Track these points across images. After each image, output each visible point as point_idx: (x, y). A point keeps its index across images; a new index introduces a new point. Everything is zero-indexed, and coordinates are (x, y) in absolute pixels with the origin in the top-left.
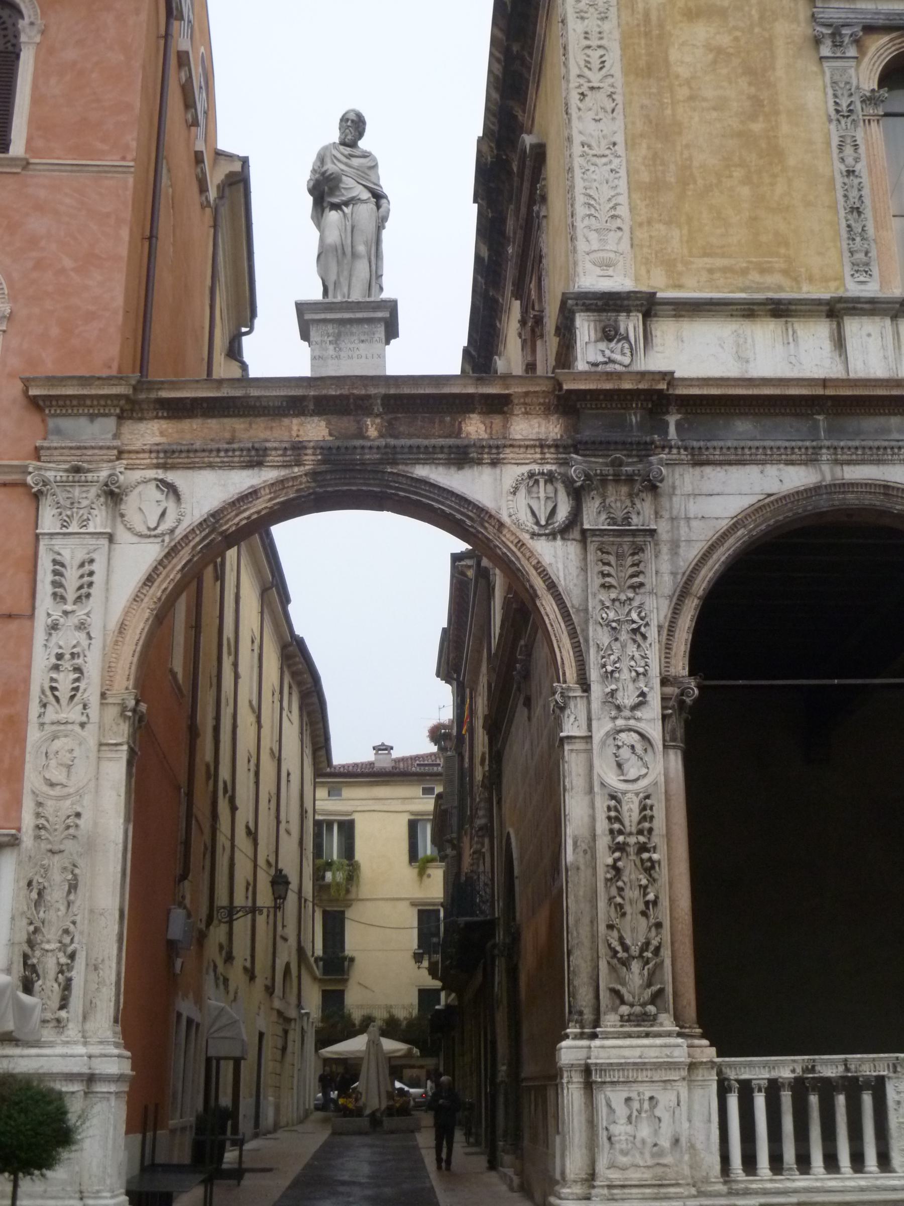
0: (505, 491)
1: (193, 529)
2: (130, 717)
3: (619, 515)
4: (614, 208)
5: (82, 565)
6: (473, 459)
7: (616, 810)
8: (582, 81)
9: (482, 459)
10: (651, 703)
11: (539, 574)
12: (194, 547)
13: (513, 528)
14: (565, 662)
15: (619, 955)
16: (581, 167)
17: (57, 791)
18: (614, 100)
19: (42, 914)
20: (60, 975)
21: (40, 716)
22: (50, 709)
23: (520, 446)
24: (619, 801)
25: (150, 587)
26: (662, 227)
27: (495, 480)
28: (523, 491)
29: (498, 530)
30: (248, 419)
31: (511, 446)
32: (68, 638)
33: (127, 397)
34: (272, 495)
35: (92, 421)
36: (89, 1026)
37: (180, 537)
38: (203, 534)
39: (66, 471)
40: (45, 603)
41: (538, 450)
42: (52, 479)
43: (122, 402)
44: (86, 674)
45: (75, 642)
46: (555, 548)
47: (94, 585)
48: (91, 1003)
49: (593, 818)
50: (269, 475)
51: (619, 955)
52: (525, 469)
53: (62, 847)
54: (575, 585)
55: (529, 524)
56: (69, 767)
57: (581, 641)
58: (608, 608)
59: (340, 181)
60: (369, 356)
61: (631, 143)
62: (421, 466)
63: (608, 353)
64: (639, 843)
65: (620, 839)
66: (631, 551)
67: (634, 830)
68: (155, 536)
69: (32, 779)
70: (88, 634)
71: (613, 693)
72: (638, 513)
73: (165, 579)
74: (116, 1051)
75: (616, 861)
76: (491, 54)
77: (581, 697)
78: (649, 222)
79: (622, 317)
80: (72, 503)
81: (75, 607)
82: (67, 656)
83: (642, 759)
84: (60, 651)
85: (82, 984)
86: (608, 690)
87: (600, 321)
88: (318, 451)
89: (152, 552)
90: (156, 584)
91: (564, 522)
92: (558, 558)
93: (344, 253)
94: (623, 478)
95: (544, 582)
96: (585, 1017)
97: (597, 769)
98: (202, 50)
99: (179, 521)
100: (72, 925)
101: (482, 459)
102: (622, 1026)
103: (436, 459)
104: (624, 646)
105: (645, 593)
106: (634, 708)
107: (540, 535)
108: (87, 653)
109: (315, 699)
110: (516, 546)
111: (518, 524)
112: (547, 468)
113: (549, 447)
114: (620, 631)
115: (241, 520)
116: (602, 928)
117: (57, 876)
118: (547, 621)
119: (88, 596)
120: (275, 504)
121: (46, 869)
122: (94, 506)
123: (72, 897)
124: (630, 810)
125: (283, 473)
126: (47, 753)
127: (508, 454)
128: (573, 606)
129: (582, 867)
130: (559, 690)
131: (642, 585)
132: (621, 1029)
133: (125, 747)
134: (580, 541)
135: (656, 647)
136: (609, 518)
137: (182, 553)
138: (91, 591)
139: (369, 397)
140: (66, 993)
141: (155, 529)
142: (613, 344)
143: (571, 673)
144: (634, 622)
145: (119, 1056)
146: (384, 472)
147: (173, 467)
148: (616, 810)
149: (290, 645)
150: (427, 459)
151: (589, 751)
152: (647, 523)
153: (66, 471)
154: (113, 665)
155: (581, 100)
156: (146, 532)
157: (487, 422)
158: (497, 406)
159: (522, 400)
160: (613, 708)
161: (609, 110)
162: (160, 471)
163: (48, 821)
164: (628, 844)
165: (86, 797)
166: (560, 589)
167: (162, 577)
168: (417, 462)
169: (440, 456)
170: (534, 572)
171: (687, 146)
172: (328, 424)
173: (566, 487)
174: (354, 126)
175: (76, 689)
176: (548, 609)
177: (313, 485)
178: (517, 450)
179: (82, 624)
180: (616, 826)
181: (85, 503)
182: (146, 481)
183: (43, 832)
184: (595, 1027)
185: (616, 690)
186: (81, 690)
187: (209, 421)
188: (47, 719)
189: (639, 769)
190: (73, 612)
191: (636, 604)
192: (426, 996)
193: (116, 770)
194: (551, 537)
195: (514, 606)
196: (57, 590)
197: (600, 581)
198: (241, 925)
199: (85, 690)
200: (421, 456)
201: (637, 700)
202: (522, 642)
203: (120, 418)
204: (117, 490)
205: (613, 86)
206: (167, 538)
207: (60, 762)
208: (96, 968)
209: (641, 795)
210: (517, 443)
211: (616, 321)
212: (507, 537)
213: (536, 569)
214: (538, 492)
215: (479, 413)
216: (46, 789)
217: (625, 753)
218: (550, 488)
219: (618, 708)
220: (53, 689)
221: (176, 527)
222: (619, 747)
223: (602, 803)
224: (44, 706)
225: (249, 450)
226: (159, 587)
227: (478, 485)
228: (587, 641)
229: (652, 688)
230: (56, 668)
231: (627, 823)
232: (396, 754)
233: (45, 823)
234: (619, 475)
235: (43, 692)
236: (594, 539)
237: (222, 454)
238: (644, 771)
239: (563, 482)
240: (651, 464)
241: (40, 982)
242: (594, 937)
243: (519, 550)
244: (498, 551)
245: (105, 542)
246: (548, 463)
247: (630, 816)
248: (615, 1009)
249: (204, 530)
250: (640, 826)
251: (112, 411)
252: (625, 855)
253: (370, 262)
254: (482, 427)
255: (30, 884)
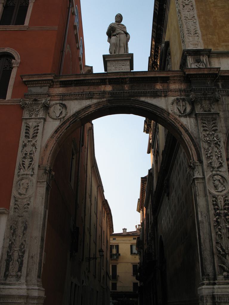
0: (169, 104)
1: (70, 117)
2: (48, 173)
3: (207, 109)
4: (196, 31)
5: (35, 127)
6: (159, 95)
7: (215, 201)
8: (183, 3)
9: (161, 95)
10: (224, 166)
11: (182, 128)
12: (70, 122)
13: (173, 114)
14: (193, 154)
15: (222, 253)
16: (185, 22)
17: (23, 196)
18: (193, 7)
19: (14, 238)
20: (19, 259)
21: (18, 173)
22: (21, 170)
23: (173, 91)
24: (216, 198)
25: (56, 134)
26: (210, 36)
27: (166, 101)
28: (175, 104)
29: (168, 115)
30: (88, 87)
31: (171, 91)
32: (28, 149)
33: (51, 80)
34: (95, 107)
35: (41, 88)
36: (28, 278)
37: (66, 119)
38: (73, 118)
39: (32, 101)
40: (22, 138)
41: (179, 92)
42: (28, 103)
43: (50, 82)
44: (34, 159)
45: (31, 150)
46: (187, 120)
47: (38, 133)
48: (30, 270)
49: (208, 205)
50: (95, 101)
51: (222, 253)
52: (175, 98)
53: (22, 215)
54: (195, 131)
55: (178, 113)
56: (27, 189)
57: (198, 147)
58: (206, 136)
59: (116, 29)
60: (125, 69)
61: (199, 17)
62: (142, 97)
63: (198, 66)
64: (225, 213)
65: (218, 211)
66: (212, 120)
67: (223, 208)
68: (58, 119)
69: (14, 193)
70: (35, 147)
71: (211, 163)
72: (213, 109)
73: (61, 132)
74: (37, 288)
75: (217, 219)
76: (153, 31)
77: (200, 165)
78: (206, 35)
79: (201, 57)
80: (33, 110)
81: (32, 140)
82: (28, 154)
83: (223, 184)
84: (26, 153)
85: (27, 263)
86: (209, 162)
87: (195, 58)
88: (110, 94)
89: (57, 123)
90: (58, 133)
91: (189, 112)
92: (188, 122)
93: (117, 46)
94: (207, 99)
95: (184, 130)
96: (210, 277)
97: (208, 188)
98: (81, 38)
99: (66, 114)
100: (24, 242)
101: (161, 95)
102: (225, 280)
103: (147, 95)
104: (213, 148)
105: (218, 132)
106: (219, 168)
107: (182, 116)
108: (35, 153)
109: (110, 215)
110: (174, 119)
111: (174, 113)
112: (182, 97)
113: (183, 91)
114: (211, 144)
115: (86, 114)
116: (214, 243)
117: (20, 224)
118: (186, 142)
119: (36, 136)
120: (96, 109)
121: (17, 222)
122: (40, 110)
123: (24, 232)
124: (221, 201)
125: (99, 100)
126: (20, 184)
127: (170, 93)
128: (194, 137)
129: (205, 222)
130: (192, 163)
131: (217, 130)
132: (225, 281)
133: (46, 183)
134: (195, 118)
135: (224, 149)
136: (204, 110)
137: (67, 124)
138: (37, 135)
139: (125, 78)
140: (21, 265)
141: (59, 117)
142: (199, 64)
143: (195, 158)
144: (215, 141)
145: (38, 289)
146: (131, 99)
147: (65, 100)
148: (215, 201)
149: (104, 201)
150: (144, 95)
151: (204, 183)
152: (216, 111)
153: (32, 101)
154: (43, 157)
155: (183, 7)
156: (56, 118)
157: (163, 85)
158: (165, 80)
159: (173, 79)
160: (211, 168)
161: (192, 9)
162: (61, 101)
163: (18, 206)
164: (221, 213)
165: (32, 198)
166: (190, 132)
167: (60, 131)
168: (141, 96)
169: (148, 94)
170: (181, 127)
171: (215, 17)
172: (113, 87)
173: (189, 102)
174: (119, 18)
175: (31, 164)
176: (186, 138)
177: (108, 104)
178: (172, 92)
179: (34, 144)
180: (216, 207)
181: (37, 110)
182: (56, 104)
183: (16, 210)
184: (214, 280)
185: (212, 162)
186: (32, 164)
187: (76, 87)
188: (21, 173)
189: (222, 188)
190: (31, 141)
191: (215, 135)
192: (135, 284)
193: (42, 190)
194: (185, 117)
195: (164, 168)
196: (26, 134)
197: (202, 129)
198: (92, 262)
199: (33, 164)
200: (142, 94)
201: (219, 165)
202: (166, 178)
203: (49, 87)
204: (47, 106)
205: (192, 4)
206: (62, 120)
207: (23, 187)
208: (32, 257)
209: (224, 196)
210: (172, 90)
211: (200, 58)
212: (171, 117)
213: (181, 126)
214: (180, 104)
215: (160, 83)
216: (18, 196)
217: (217, 183)
218: (184, 103)
219: (213, 168)
220: (23, 164)
221: (65, 116)
222: (214, 181)
223: (210, 199)
224: (20, 169)
225: (88, 94)
226: (59, 134)
227: (161, 103)
228: (200, 147)
229: (224, 161)
230: (24, 158)
231: (220, 206)
232: (128, 231)
233: (17, 207)
234: (204, 99)
235: (20, 165)
236: (200, 116)
237: (80, 95)
238: (224, 188)
239: (188, 101)
240: (216, 94)
241: (12, 262)
242: (212, 247)
243: (175, 121)
244: (169, 121)
245: (42, 120)
246: (182, 96)
247: (221, 203)
248: (221, 274)
249: (74, 117)
250: (224, 207)
251: (47, 85)
252: (220, 217)
253: (125, 49)
254: (161, 87)
255: (11, 227)
